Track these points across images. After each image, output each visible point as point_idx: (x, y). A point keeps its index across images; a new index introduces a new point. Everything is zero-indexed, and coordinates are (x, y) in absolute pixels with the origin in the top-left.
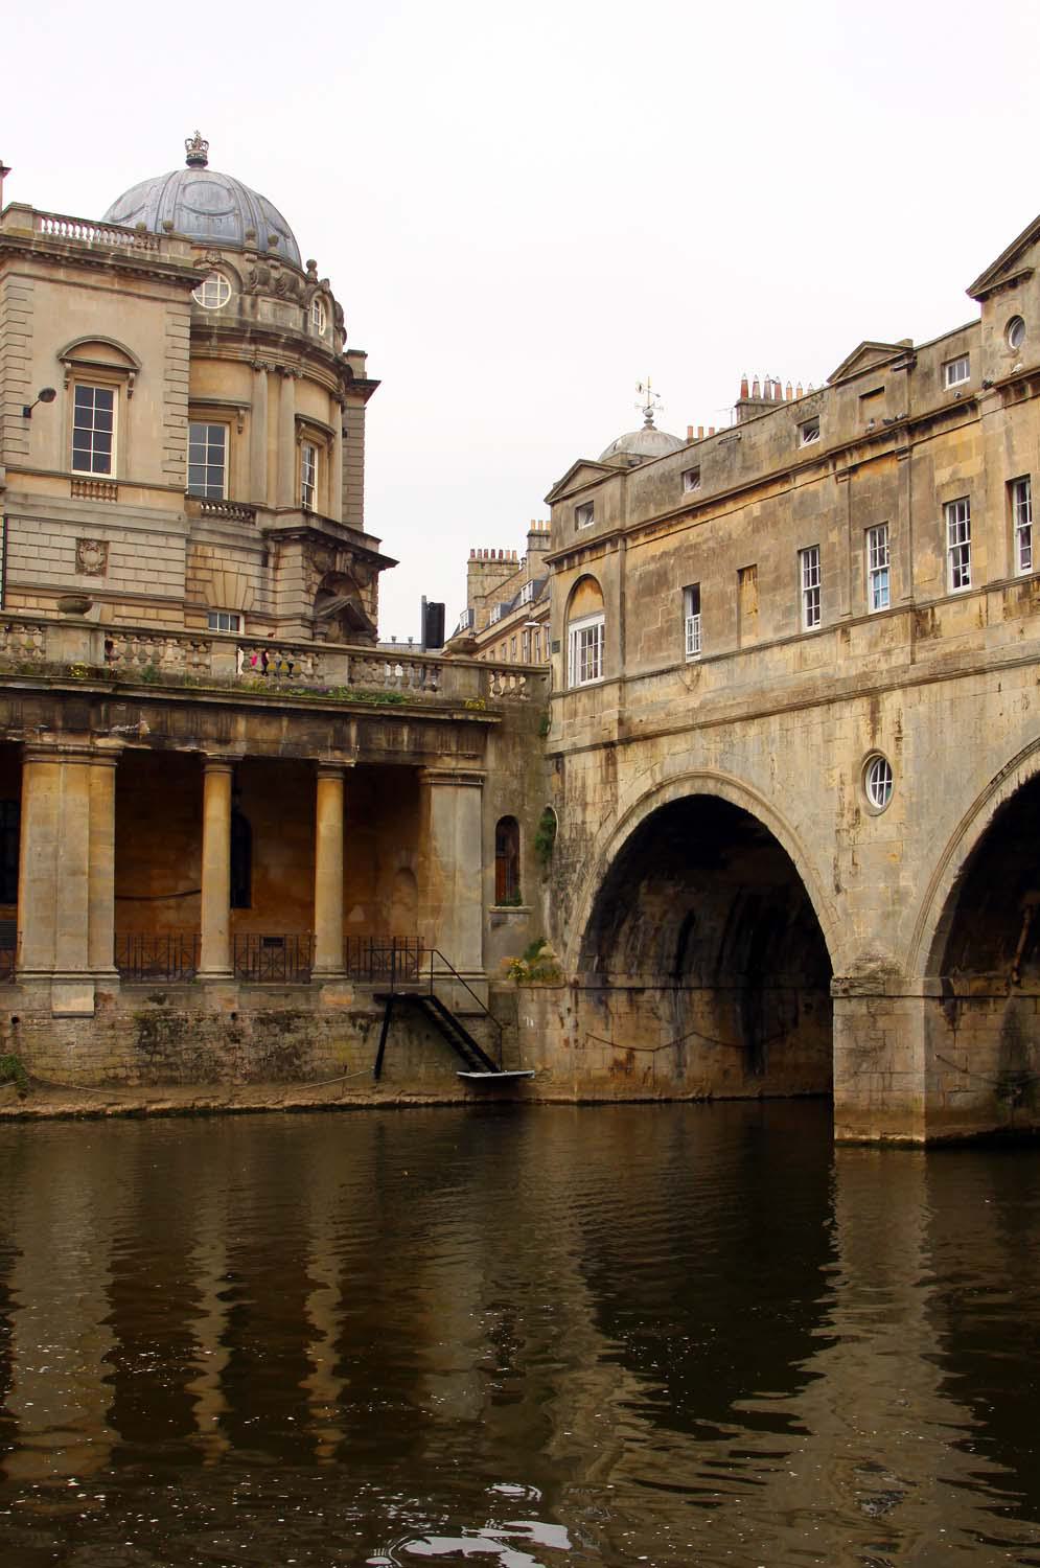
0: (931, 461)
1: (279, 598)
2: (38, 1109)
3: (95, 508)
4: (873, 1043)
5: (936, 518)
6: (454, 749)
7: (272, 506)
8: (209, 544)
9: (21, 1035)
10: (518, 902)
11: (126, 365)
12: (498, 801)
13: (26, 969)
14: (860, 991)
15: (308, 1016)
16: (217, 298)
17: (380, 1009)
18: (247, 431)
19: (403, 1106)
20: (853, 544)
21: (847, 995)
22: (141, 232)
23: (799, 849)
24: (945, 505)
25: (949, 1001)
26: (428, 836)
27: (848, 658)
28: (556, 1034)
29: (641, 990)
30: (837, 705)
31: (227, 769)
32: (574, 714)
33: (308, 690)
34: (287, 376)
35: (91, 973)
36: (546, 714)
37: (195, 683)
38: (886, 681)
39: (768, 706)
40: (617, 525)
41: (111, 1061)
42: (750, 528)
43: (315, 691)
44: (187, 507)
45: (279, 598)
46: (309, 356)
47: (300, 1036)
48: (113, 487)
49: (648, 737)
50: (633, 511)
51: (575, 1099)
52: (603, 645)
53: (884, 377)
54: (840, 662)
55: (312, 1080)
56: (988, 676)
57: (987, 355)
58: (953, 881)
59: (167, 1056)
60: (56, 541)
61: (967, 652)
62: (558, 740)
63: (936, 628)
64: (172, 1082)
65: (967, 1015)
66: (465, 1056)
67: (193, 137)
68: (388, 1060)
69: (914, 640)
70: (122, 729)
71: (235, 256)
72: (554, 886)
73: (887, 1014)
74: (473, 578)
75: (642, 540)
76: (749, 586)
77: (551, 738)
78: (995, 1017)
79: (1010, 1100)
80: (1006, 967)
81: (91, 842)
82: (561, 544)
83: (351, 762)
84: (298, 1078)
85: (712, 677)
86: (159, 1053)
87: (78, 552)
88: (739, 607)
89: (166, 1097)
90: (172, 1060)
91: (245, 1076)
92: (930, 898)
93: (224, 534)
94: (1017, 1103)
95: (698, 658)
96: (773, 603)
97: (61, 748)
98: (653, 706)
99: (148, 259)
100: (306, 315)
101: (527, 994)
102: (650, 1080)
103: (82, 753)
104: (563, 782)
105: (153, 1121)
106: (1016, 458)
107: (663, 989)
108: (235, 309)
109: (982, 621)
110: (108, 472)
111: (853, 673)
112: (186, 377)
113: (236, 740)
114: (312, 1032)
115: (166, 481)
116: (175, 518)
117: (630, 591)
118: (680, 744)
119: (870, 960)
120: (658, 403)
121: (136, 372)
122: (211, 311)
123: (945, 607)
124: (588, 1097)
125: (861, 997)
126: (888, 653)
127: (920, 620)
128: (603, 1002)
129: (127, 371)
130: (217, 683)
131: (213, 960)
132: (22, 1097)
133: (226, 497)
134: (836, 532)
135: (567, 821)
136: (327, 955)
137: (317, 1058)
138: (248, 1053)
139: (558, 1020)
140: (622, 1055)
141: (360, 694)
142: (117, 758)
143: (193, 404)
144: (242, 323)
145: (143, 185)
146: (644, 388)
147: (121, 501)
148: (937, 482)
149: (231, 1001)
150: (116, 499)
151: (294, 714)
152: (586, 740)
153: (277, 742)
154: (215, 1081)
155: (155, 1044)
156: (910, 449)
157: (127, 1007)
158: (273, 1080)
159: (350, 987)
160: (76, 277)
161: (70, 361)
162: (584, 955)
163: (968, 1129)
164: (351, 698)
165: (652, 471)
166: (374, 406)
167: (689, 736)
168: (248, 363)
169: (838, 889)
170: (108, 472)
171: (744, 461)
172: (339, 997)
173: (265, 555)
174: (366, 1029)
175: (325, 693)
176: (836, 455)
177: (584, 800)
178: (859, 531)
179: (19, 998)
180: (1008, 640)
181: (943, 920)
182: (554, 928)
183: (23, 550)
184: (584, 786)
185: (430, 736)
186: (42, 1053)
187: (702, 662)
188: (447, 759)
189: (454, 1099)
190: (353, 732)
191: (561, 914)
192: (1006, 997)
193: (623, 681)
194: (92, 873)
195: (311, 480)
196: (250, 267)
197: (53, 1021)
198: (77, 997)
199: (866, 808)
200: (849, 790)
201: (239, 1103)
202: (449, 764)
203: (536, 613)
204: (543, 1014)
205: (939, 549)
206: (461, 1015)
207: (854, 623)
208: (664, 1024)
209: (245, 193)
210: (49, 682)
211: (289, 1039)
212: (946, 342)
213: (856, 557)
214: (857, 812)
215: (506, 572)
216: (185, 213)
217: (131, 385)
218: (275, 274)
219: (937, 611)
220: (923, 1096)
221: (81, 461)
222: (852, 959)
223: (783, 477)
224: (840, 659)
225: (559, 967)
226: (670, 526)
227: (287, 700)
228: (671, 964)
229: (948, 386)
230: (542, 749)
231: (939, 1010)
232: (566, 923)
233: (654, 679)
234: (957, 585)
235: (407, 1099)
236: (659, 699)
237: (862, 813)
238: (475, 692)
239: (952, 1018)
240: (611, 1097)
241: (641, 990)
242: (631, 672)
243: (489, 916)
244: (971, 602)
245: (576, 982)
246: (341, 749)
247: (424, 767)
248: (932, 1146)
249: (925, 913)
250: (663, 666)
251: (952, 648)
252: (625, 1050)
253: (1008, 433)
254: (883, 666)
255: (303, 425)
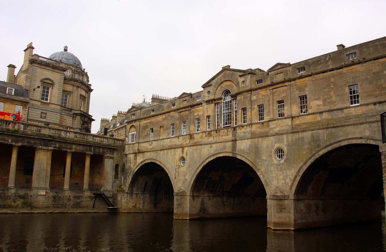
0: (194, 112)
1: (75, 125)
2: (34, 212)
3: (45, 107)
4: (181, 203)
5: (194, 121)
6: (109, 152)
7: (75, 109)
8: (64, 115)
9: (32, 198)
10: (118, 179)
11: (52, 83)
12: (116, 161)
13: (34, 187)
14: (179, 195)
15: (82, 197)
16: (68, 73)
17: (94, 196)
18: (72, 96)
19: (97, 212)
20: (180, 124)
21: (177, 195)
22: (55, 61)
23: (169, 172)
24: (196, 119)
25: (193, 197)
26: (104, 167)
27: (179, 141)
28: (123, 201)
29: (138, 194)
30: (176, 149)
31: (71, 154)
32: (130, 148)
33: (86, 141)
34: (79, 88)
35: (45, 188)
36: (124, 147)
37: (67, 139)
38: (185, 146)
39: (165, 148)
40: (139, 118)
41: (47, 203)
42: (162, 120)
43: (87, 141)
44: (61, 108)
45: (75, 125)
46: (83, 84)
47: (81, 200)
48: (48, 104)
49: (143, 152)
50: (142, 115)
51: (126, 212)
52: (135, 137)
53: (187, 98)
54: (177, 142)
55: (82, 208)
56: (202, 146)
57: (204, 96)
58: (195, 177)
59: (57, 203)
60: (37, 112)
61: (199, 142)
62: (127, 152)
63: (194, 138)
64: (58, 207)
65: (196, 199)
66: (108, 204)
67: (65, 46)
68: (95, 204)
69: (190, 139)
70: (53, 146)
71: (72, 67)
72: (124, 176)
73: (184, 198)
74: (101, 123)
75: (143, 120)
76: (162, 129)
77: (125, 151)
78: (200, 199)
79: (202, 213)
80: (202, 191)
81: (47, 165)
82: (129, 120)
83: (92, 154)
84: (80, 207)
85: (155, 143)
86: (56, 202)
87: (41, 114)
88: (160, 132)
89: (57, 210)
90: (58, 204)
91: (71, 207)
92: (191, 180)
93: (66, 113)
94: (203, 213)
95: (152, 140)
96: (166, 132)
97: (43, 148)
98: (144, 147)
99: (58, 66)
100: (83, 78)
101: (119, 194)
102: (139, 209)
103: (47, 150)
104: (127, 159)
105: (54, 214)
106: (208, 112)
107: (141, 194)
108: (71, 76)
109: (202, 137)
110: (47, 101)
111: (179, 144)
112: (62, 86)
113: (73, 149)
114: (83, 199)
115: (57, 103)
116: (59, 110)
117: (141, 128)
118: (149, 154)
119: (181, 190)
120: (146, 98)
121: (54, 84)
122: (67, 75)
123: (195, 135)
124: (128, 212)
125: (179, 196)
126: (185, 141)
127: (191, 136)
128: (132, 196)
129: (52, 84)
130: (70, 139)
131: (66, 186)
132: (31, 209)
133: (67, 107)
134: (177, 122)
135: (127, 165)
136: (86, 186)
137: (84, 204)
138: (71, 203)
139: (124, 198)
140: (134, 205)
141: (94, 142)
142: (52, 151)
143: (64, 91)
144: (72, 78)
145: (56, 53)
146: (144, 95)
147: (49, 106)
148: (195, 115)
149: (69, 194)
150: (49, 106)
151: (83, 145)
152: (132, 152)
153: (80, 150)
154: (66, 207)
155: (56, 201)
156: (191, 110)
157: (51, 194)
158: (76, 207)
159: (89, 192)
160: (45, 68)
161: (43, 82)
162: (129, 188)
163: (195, 217)
164: (93, 143)
165: (146, 109)
166: (92, 93)
167: (150, 152)
168: (72, 85)
169: (175, 178)
170: (47, 101)
171: (162, 109)
172: (87, 194)
173: (73, 117)
174: (92, 199)
175: (88, 142)
176: (178, 109)
177: (131, 162)
178: (181, 122)
179: (32, 192)
180: (206, 140)
181: (193, 183)
182: (124, 183)
183: (32, 113)
184: (131, 160)
185: (105, 150)
186: (35, 202)
187: (153, 141)
188: (108, 154)
189: (106, 212)
190: (93, 149)
191: (125, 181)
192: (201, 196)
193: (139, 143)
194: (47, 170)
195: (81, 105)
196: (74, 69)
197: (38, 196)
198: (42, 192)
199: (181, 166)
200: (178, 162)
201: (70, 211)
202: (108, 155)
203: (113, 130)
204: (121, 198)
205: (195, 126)
206: (108, 197)
207: (180, 136)
208: (141, 200)
209: (74, 57)
210: (41, 137)
211: (79, 200)
212: (197, 94)
213: (181, 126)
214: (179, 166)
215: (107, 122)
216: (63, 59)
217: (53, 87)
218: (78, 70)
219: (194, 135)
220: (189, 212)
221: (43, 99)
222: (177, 189)
223: (169, 112)
224: (178, 142)
225: (124, 190)
226: (149, 118)
227: (82, 143)
228: (143, 190)
229: (197, 100)
230: (124, 153)
231: (191, 198)
232: (126, 182)
233: (144, 143)
234: (197, 131)
235: (98, 211)
236: (145, 146)
237: (180, 166)
238: (113, 143)
239: (194, 199)
240: (132, 212)
241: (138, 194)
242: (140, 141)
243: (113, 181)
244: (200, 134)
245: (127, 192)
246: (91, 152)
247: (104, 155)
248: (190, 220)
249: (190, 183)
250: (146, 141)
251: (196, 141)
252: (310, 111)
253: (207, 108)
254: (185, 143)
255: (81, 96)
